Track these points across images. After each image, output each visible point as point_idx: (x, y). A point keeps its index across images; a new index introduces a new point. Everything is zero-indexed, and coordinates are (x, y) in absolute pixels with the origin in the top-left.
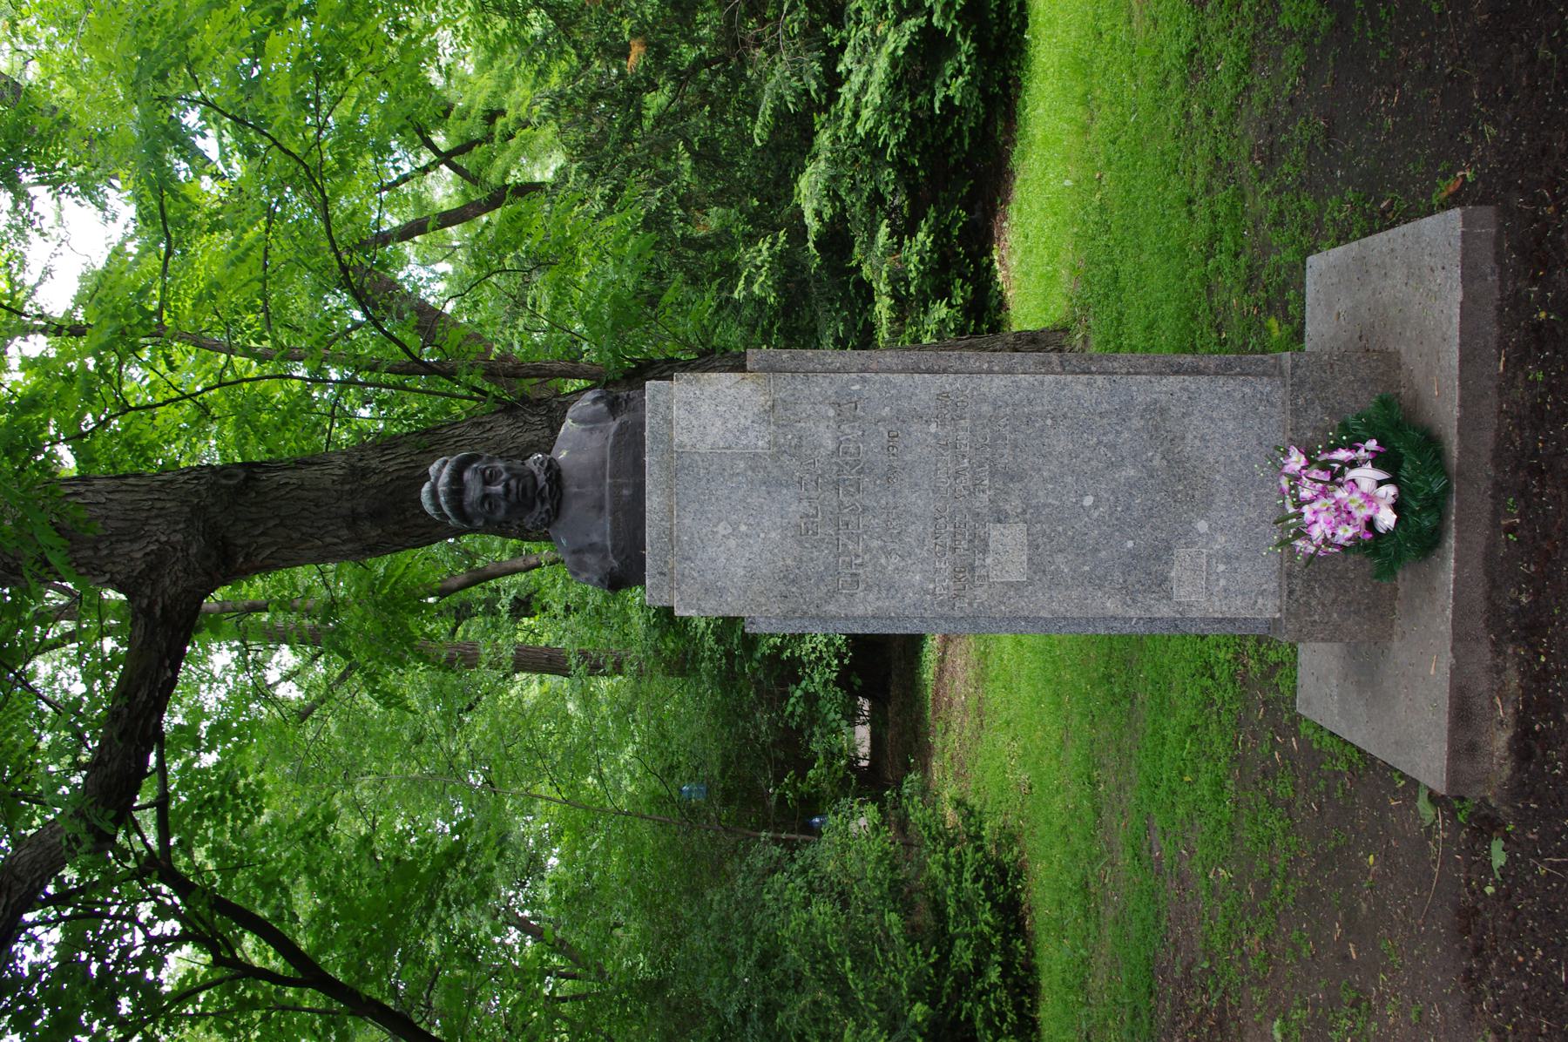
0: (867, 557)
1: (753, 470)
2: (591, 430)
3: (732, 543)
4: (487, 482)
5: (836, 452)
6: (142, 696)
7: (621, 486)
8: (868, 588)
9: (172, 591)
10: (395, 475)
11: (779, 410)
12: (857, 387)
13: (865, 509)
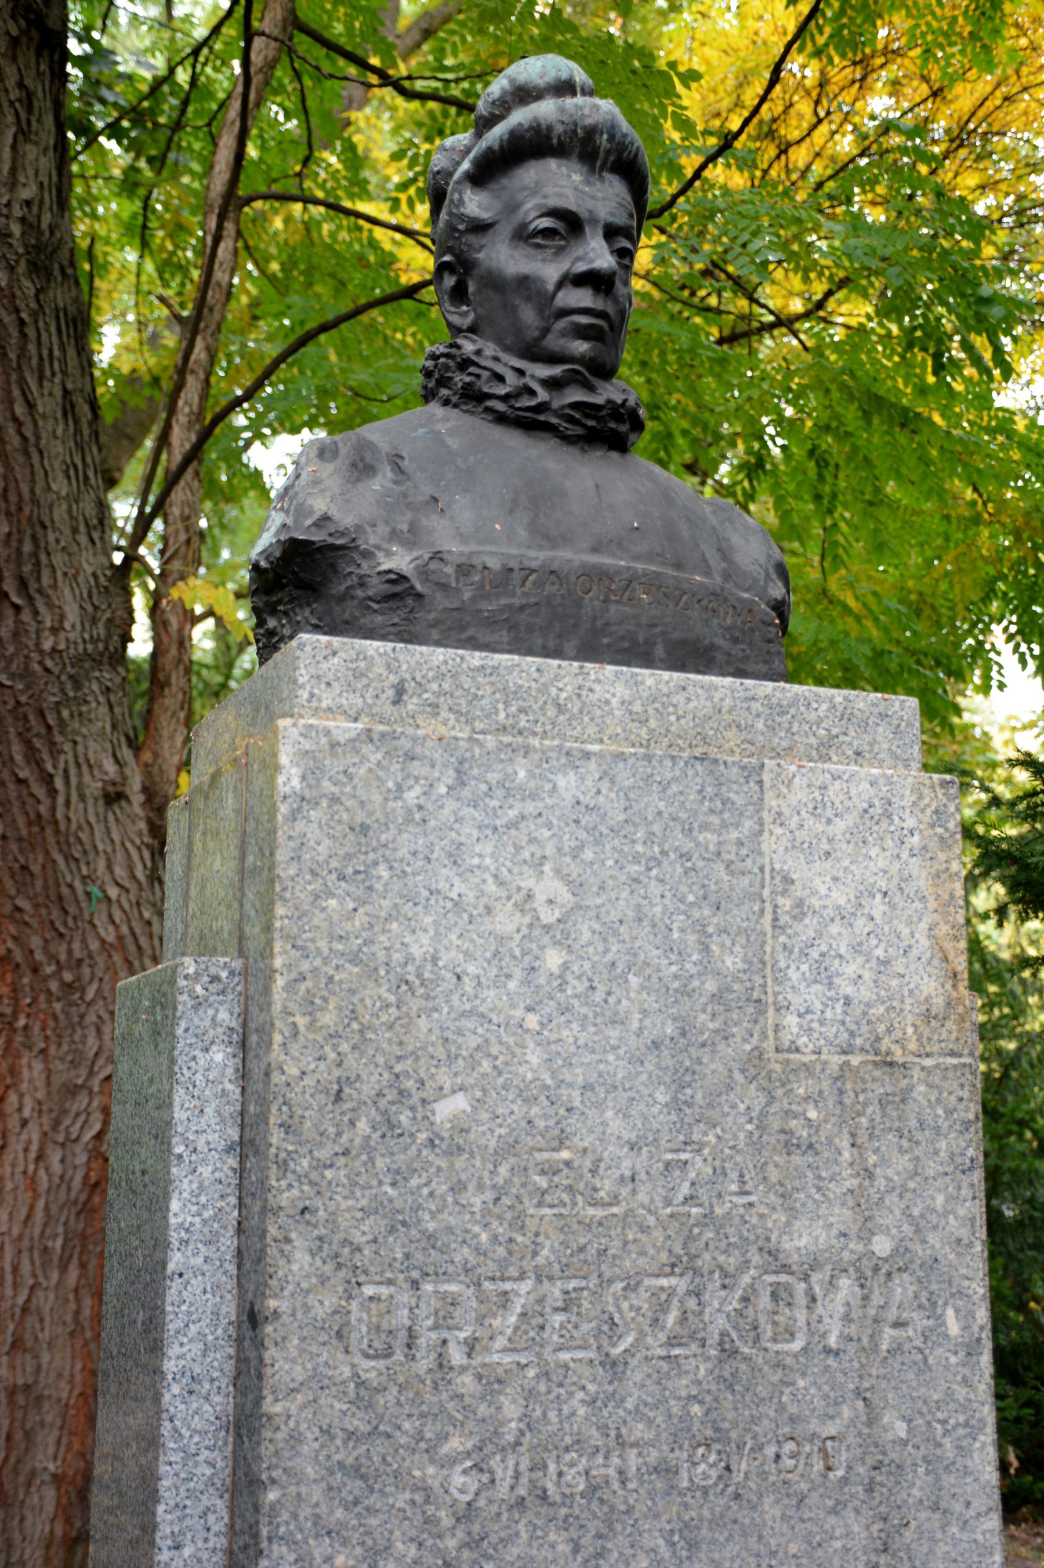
0: (466, 1383)
1: (717, 997)
3: (507, 922)
5: (775, 1259)
8: (363, 1394)
10: (31, 333)
11: (882, 1085)
12: (953, 1327)
13: (614, 1367)
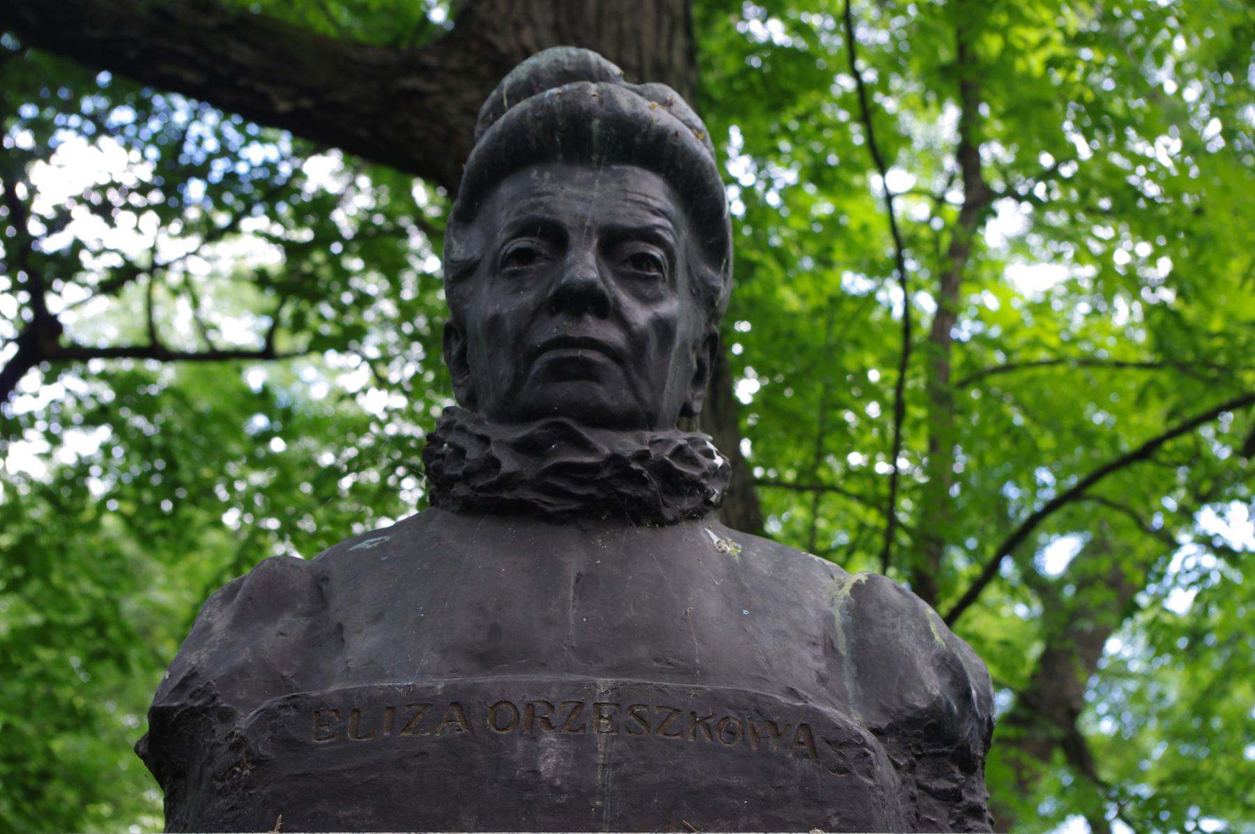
2: (830, 648)
4: (614, 242)
6: (241, 53)
7: (576, 732)
9: (452, 108)
